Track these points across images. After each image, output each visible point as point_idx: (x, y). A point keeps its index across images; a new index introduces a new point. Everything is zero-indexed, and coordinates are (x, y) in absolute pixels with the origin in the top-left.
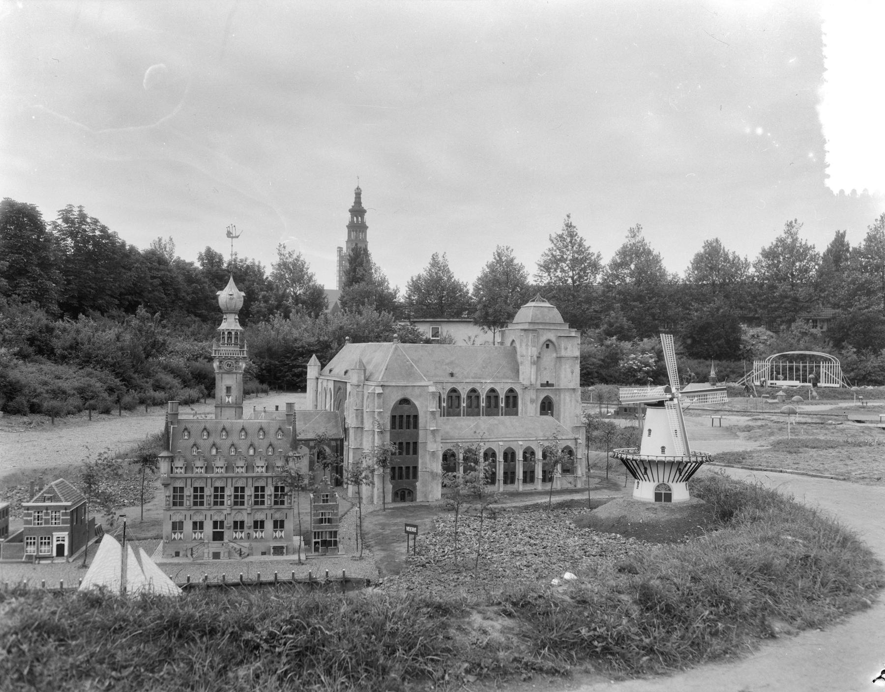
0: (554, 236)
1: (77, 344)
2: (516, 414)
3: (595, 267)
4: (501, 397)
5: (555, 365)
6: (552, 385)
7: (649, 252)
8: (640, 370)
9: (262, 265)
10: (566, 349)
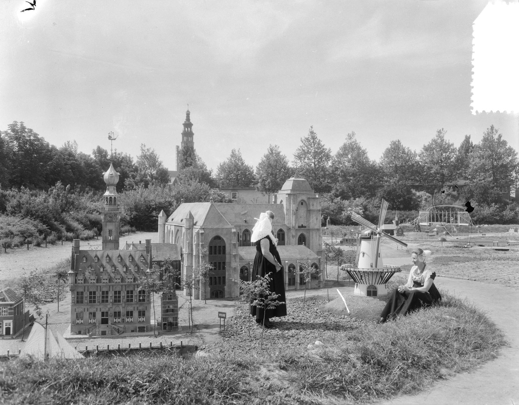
0: (303, 138)
2: (284, 244)
3: (328, 157)
6: (305, 227)
7: (359, 148)
9: (131, 156)
10: (313, 205)
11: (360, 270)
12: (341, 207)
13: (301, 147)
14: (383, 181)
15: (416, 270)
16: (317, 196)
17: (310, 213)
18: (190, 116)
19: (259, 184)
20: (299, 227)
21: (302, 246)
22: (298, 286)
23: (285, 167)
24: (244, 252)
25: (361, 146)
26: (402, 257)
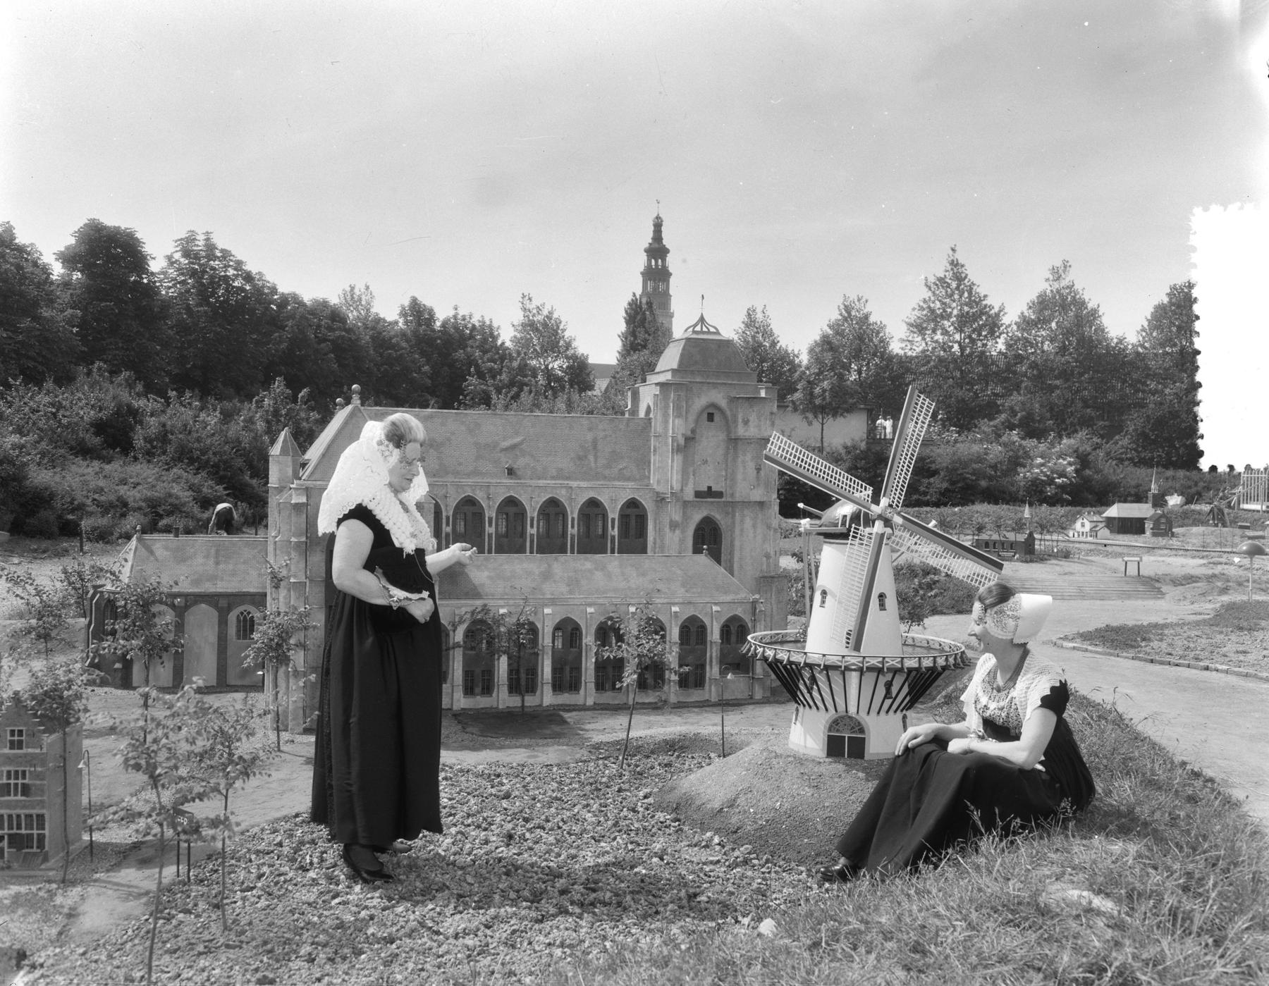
0: (932, 279)
1: (166, 433)
2: (643, 550)
3: (993, 326)
4: (611, 516)
5: (726, 454)
6: (719, 494)
7: (1082, 304)
8: (1051, 481)
9: (495, 325)
10: (746, 422)
11: (814, 658)
12: (1018, 457)
13: (925, 301)
14: (1144, 392)
15: (992, 675)
16: (763, 394)
17: (735, 449)
18: (663, 229)
19: (798, 395)
20: (698, 494)
21: (703, 559)
22: (672, 691)
23: (883, 354)
24: (486, 573)
25: (1086, 297)
26: (1129, 597)
